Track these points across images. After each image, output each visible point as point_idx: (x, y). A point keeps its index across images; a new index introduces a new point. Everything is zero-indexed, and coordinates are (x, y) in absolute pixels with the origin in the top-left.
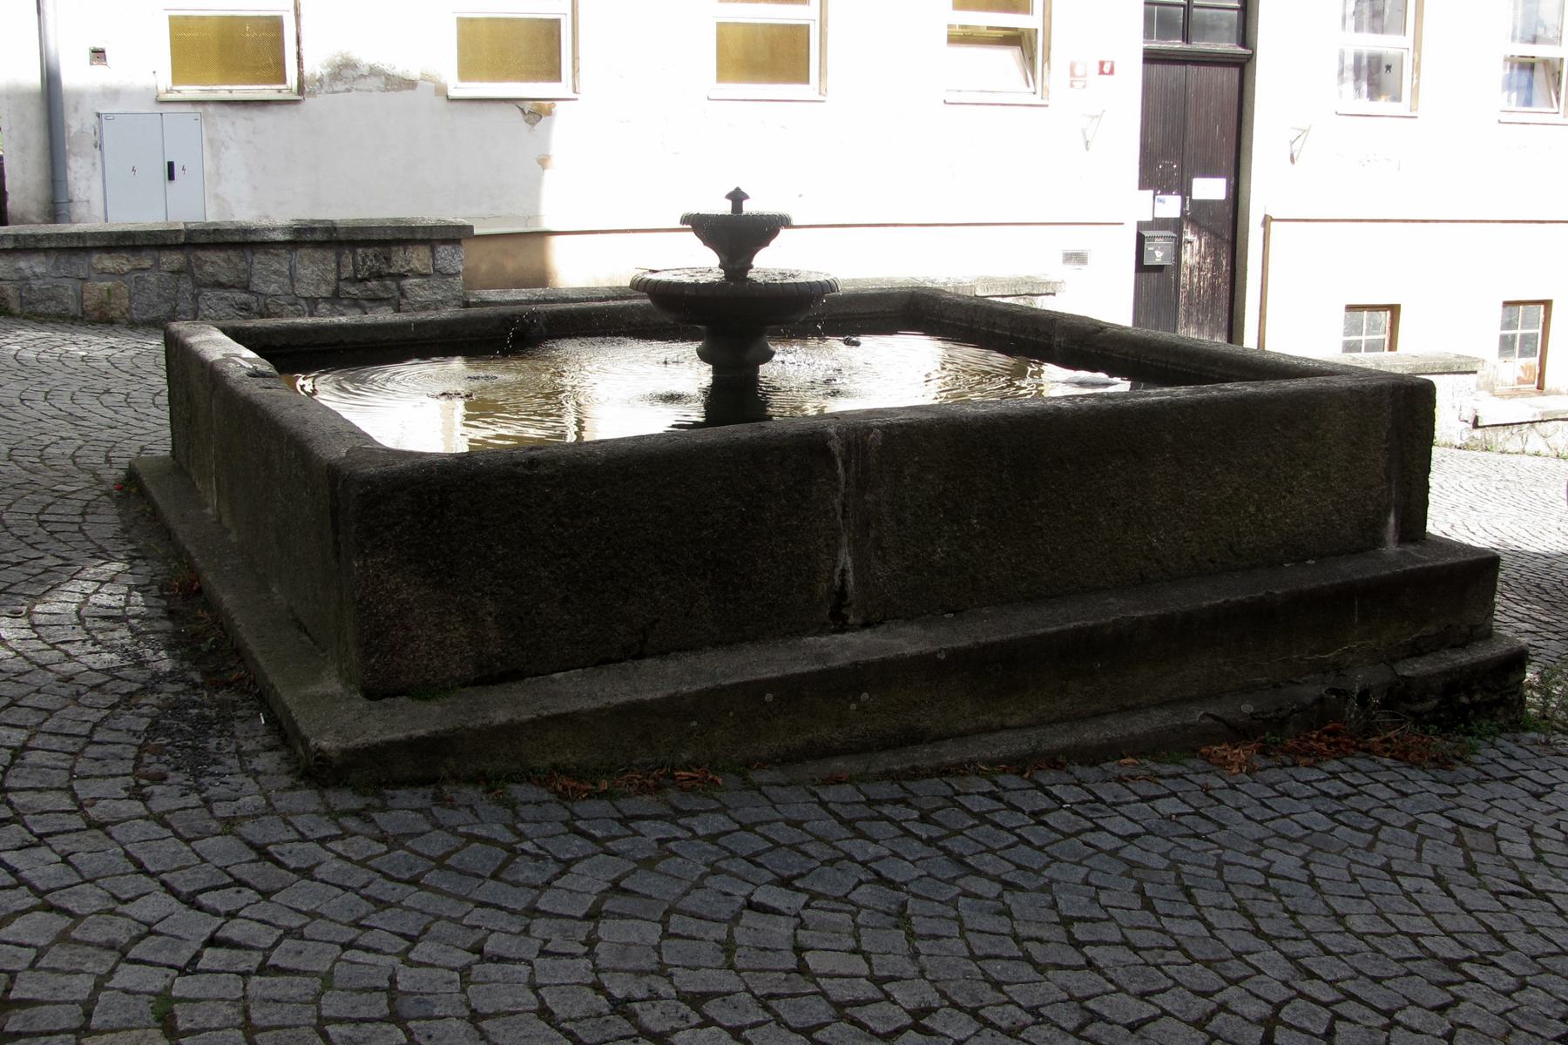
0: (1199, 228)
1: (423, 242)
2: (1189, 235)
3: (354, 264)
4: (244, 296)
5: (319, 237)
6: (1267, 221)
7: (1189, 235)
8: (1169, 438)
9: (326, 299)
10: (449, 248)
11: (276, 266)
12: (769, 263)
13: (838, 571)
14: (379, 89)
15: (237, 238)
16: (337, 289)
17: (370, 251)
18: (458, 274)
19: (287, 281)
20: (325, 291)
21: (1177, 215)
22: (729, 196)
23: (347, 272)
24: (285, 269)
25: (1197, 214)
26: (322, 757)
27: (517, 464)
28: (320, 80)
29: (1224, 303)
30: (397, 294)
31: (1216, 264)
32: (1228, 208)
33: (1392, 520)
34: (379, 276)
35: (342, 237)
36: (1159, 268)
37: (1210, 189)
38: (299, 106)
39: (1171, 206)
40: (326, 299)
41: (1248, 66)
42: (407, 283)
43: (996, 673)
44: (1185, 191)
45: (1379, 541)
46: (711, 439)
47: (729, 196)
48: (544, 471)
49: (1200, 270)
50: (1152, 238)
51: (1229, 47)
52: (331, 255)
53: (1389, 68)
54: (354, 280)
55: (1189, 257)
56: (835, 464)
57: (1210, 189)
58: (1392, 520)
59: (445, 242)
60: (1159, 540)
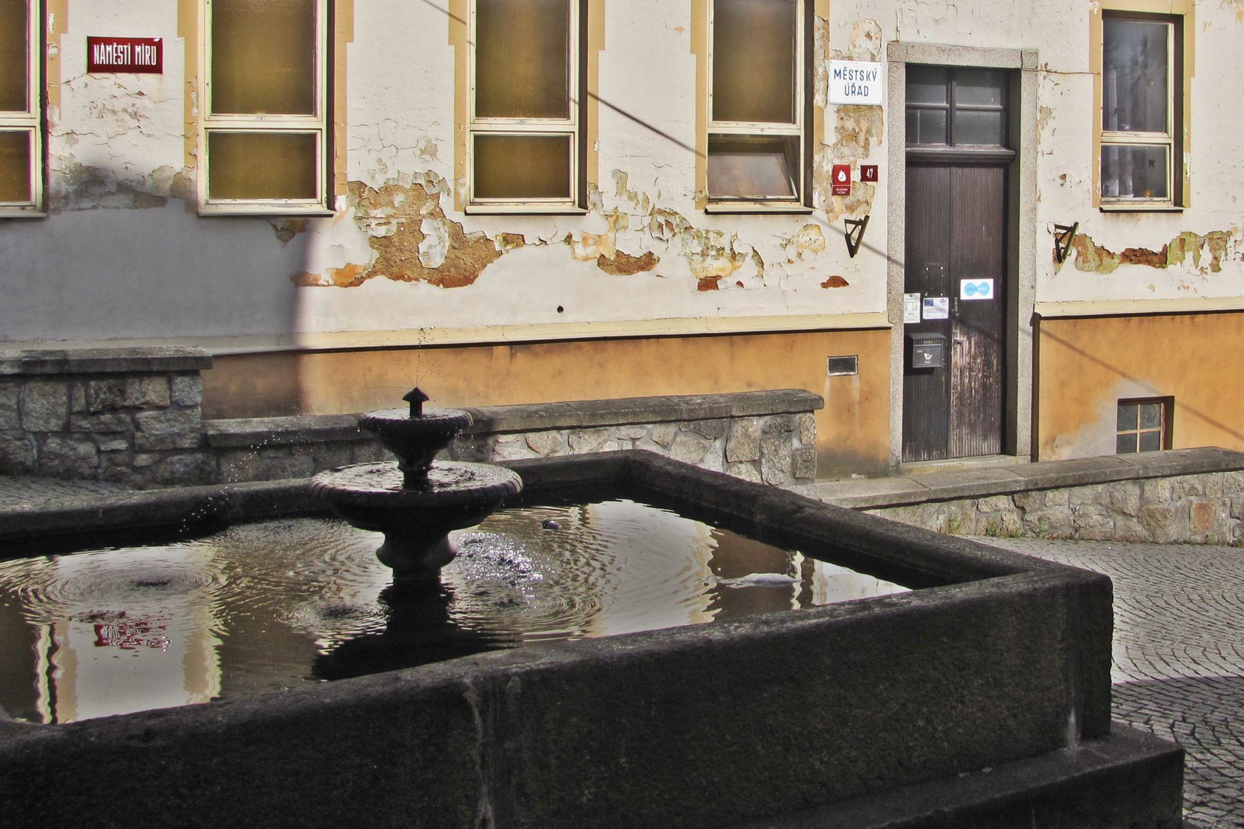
0: (968, 329)
1: (160, 374)
2: (958, 336)
3: (87, 396)
5: (49, 369)
6: (1036, 319)
7: (958, 336)
8: (828, 661)
9: (55, 434)
10: (186, 379)
13: (478, 821)
14: (127, 206)
17: (104, 384)
18: (195, 406)
19: (14, 415)
20: (54, 425)
22: (407, 398)
23: (79, 405)
24: (13, 402)
25: (964, 314)
27: (131, 738)
28: (66, 197)
29: (996, 402)
30: (132, 427)
31: (987, 363)
32: (997, 308)
33: (1072, 719)
34: (113, 409)
35: (74, 369)
36: (929, 371)
37: (978, 289)
38: (44, 223)
39: (939, 309)
40: (55, 434)
42: (143, 416)
46: (342, 696)
47: (407, 398)
48: (159, 742)
49: (971, 370)
50: (921, 341)
51: (991, 148)
52: (62, 388)
53: (1152, 163)
54: (86, 414)
55: (959, 358)
56: (472, 714)
57: (978, 289)
58: (1072, 719)
59: (183, 373)
60: (822, 762)
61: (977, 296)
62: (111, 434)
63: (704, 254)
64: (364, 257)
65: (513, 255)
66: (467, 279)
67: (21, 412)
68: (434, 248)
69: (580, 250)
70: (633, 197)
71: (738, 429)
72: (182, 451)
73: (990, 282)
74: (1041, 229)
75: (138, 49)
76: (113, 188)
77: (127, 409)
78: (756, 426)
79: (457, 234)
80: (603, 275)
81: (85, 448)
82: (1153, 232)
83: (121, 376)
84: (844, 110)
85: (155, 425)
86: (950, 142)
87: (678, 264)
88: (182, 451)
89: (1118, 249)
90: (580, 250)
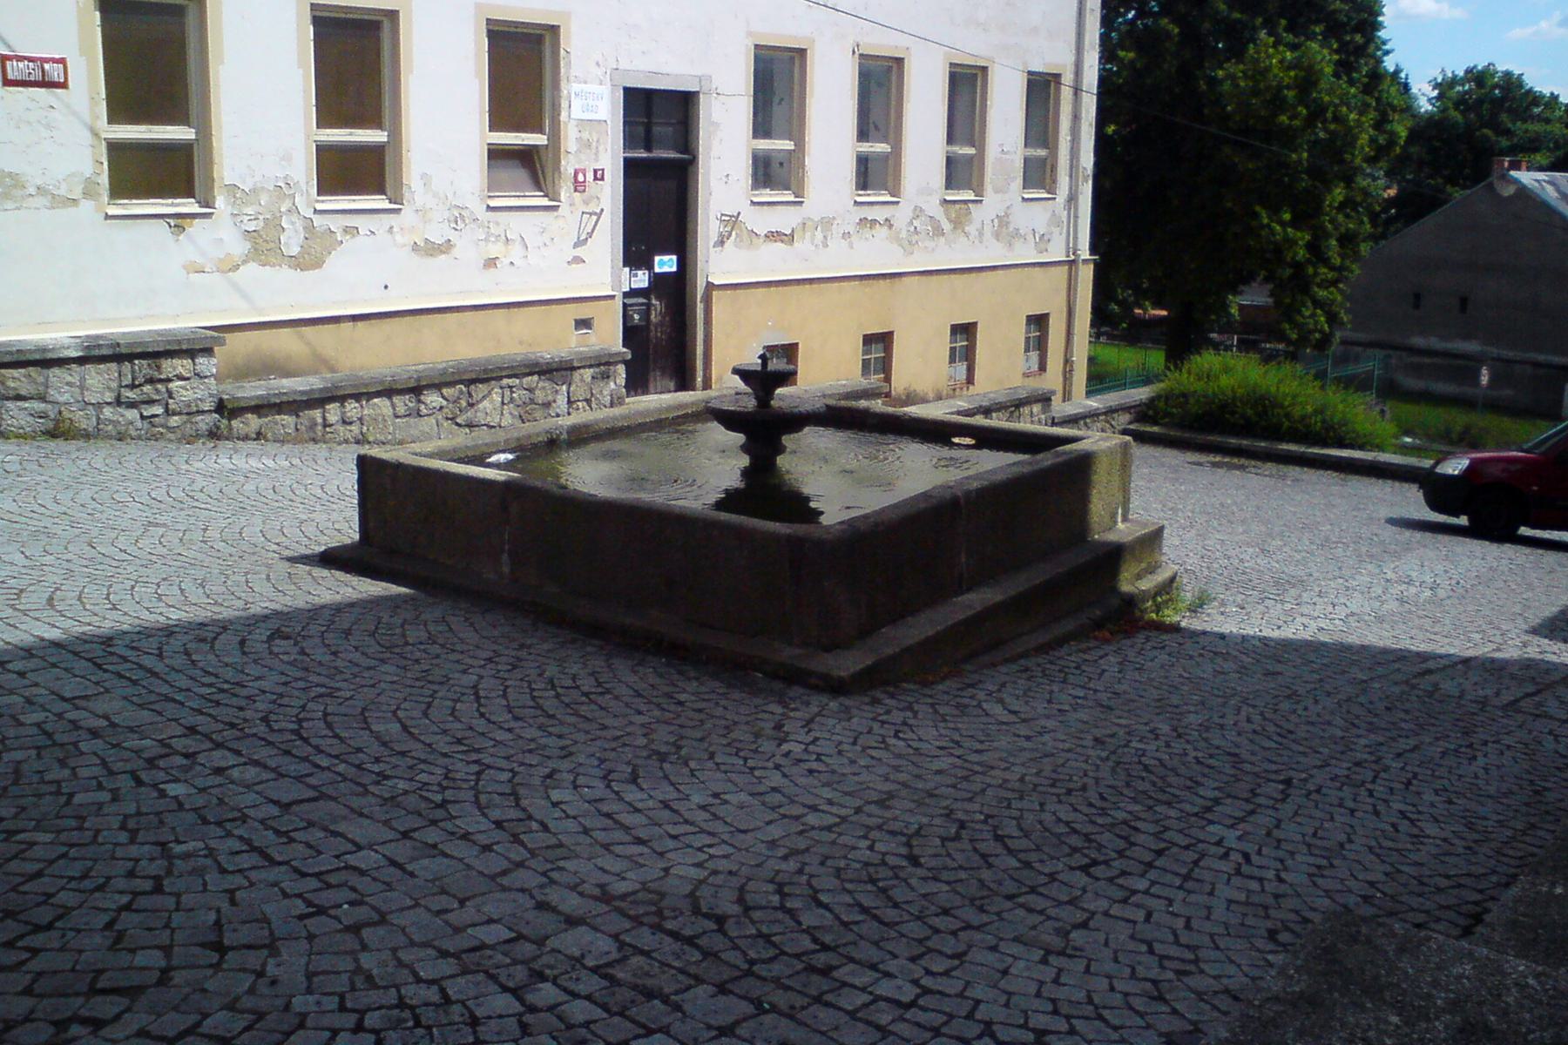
3: (133, 372)
4: (42, 406)
5: (105, 352)
11: (69, 379)
12: (783, 395)
15: (38, 357)
16: (119, 396)
21: (646, 284)
23: (127, 380)
24: (75, 379)
25: (658, 281)
26: (841, 680)
34: (151, 381)
35: (124, 351)
37: (666, 263)
39: (642, 280)
41: (691, 169)
43: (1019, 607)
44: (650, 267)
45: (1115, 523)
52: (114, 366)
54: (133, 386)
57: (666, 263)
61: (666, 269)
62: (151, 402)
63: (486, 240)
64: (239, 247)
65: (349, 243)
66: (318, 264)
67: (82, 388)
68: (292, 242)
69: (399, 238)
70: (435, 195)
71: (577, 375)
72: (203, 412)
73: (674, 258)
74: (712, 218)
75: (47, 66)
76: (32, 190)
77: (161, 381)
78: (588, 373)
79: (309, 227)
80: (416, 259)
81: (132, 414)
82: (783, 219)
83: (155, 356)
84: (581, 122)
85: (185, 393)
86: (648, 149)
87: (468, 248)
88: (203, 412)
89: (762, 231)
90: (399, 238)
